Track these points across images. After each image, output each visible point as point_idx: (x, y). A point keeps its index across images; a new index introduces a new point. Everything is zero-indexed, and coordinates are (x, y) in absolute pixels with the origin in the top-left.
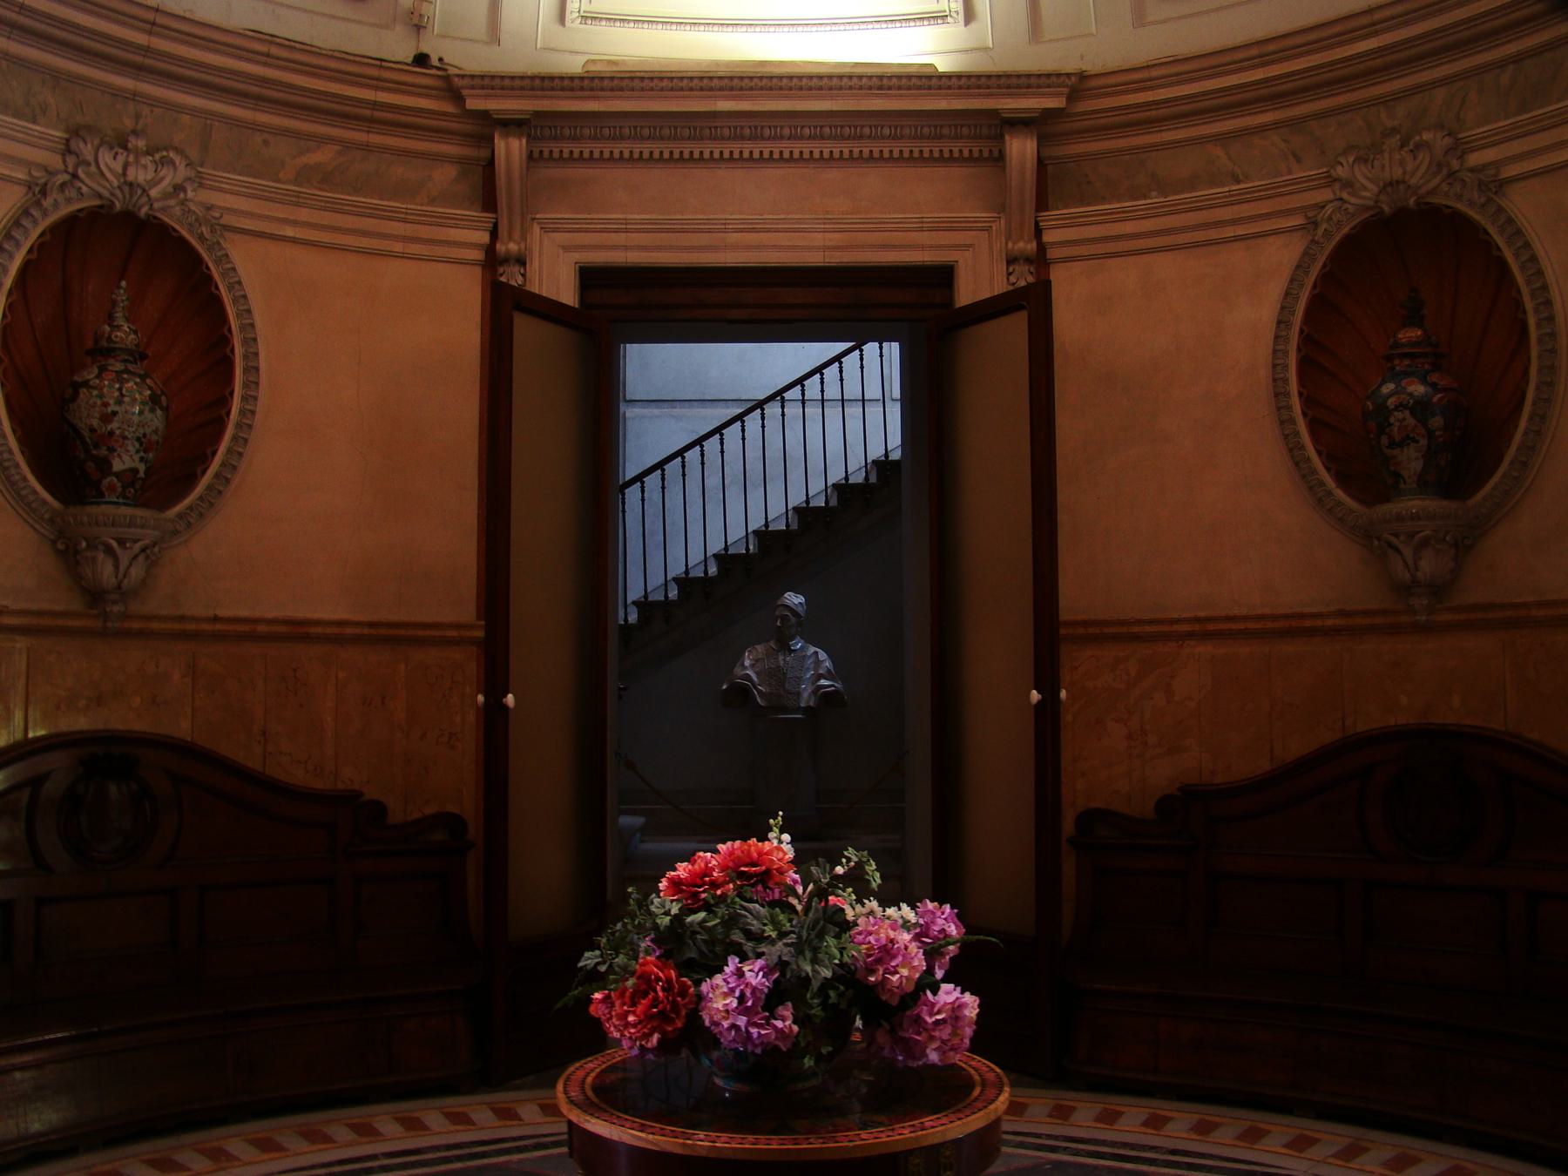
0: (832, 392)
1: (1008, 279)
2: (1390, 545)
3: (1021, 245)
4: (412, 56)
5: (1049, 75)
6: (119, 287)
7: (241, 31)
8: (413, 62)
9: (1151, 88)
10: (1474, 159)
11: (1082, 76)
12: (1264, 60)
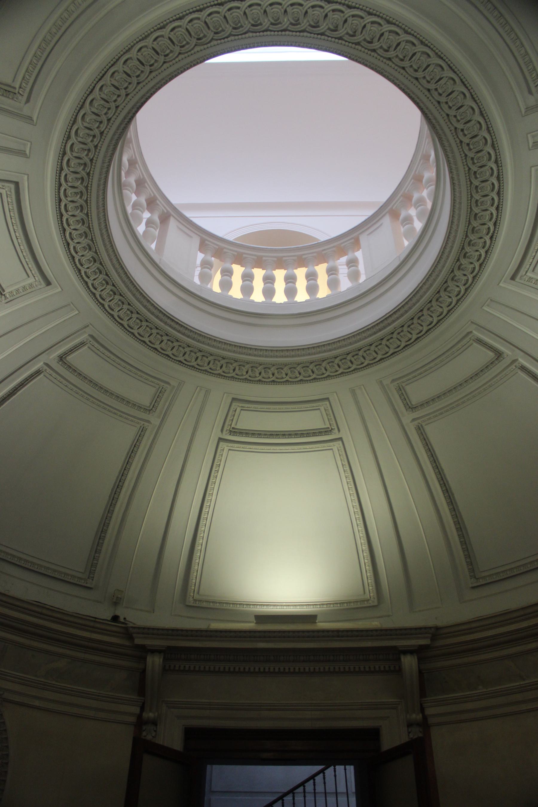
0: (320, 788)
1: (409, 735)
3: (414, 716)
4: (111, 616)
5: (420, 628)
7: (31, 602)
8: (111, 619)
9: (473, 633)
11: (437, 628)
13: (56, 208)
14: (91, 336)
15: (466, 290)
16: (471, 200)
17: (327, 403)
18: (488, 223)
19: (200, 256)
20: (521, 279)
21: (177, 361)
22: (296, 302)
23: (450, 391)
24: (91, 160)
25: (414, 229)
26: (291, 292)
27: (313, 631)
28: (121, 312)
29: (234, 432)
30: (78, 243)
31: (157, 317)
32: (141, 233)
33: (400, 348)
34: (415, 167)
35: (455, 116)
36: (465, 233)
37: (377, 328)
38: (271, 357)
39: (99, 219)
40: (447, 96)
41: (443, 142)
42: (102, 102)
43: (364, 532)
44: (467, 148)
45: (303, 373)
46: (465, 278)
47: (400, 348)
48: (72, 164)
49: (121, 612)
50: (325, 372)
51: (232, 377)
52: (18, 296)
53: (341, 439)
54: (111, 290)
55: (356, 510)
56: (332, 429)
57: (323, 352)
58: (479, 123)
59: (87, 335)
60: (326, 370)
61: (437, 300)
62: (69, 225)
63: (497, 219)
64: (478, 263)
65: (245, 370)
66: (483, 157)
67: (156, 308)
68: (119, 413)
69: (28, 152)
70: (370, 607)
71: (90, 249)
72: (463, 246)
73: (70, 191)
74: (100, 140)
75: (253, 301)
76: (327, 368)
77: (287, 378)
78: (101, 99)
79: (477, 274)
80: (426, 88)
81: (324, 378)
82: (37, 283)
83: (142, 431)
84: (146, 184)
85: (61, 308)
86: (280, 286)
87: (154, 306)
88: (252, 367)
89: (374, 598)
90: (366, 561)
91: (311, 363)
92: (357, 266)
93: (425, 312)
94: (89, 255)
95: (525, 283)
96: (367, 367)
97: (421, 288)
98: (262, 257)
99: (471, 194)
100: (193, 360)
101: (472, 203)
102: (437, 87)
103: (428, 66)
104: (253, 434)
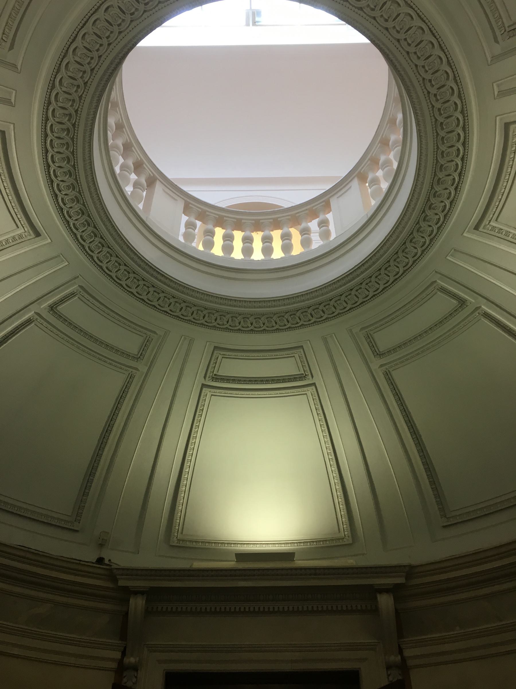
1: (388, 678)
7: (15, 546)
8: (96, 562)
11: (411, 567)
13: (43, 158)
14: (81, 287)
15: (431, 240)
16: (437, 151)
17: (302, 350)
18: (453, 174)
19: (185, 218)
20: (484, 228)
21: (163, 311)
22: (273, 259)
23: (415, 338)
24: (76, 111)
25: (381, 189)
26: (267, 250)
27: (291, 569)
28: (109, 264)
29: (216, 378)
30: (66, 195)
31: (144, 269)
32: (129, 193)
33: (368, 298)
34: (382, 132)
35: (423, 67)
36: (431, 184)
37: (347, 279)
38: (250, 307)
39: (85, 170)
40: (416, 46)
41: (411, 94)
42: (85, 51)
43: (337, 472)
44: (435, 99)
45: (278, 322)
46: (431, 229)
47: (368, 298)
48: (57, 114)
49: (107, 555)
50: (299, 321)
51: (214, 326)
52: (8, 245)
53: (314, 384)
54: (100, 243)
55: (329, 451)
56: (306, 375)
57: (297, 303)
58: (447, 73)
59: (77, 285)
60: (300, 319)
61: (403, 251)
62: (56, 177)
63: (462, 169)
64: (436, 226)
65: (225, 320)
66: (450, 107)
67: (143, 261)
68: (109, 361)
69: (13, 101)
70: (346, 545)
71: (78, 202)
72: (429, 198)
73: (56, 142)
74: (84, 91)
75: (233, 259)
76: (301, 318)
77: (265, 327)
78: (83, 48)
79: (442, 225)
80: (395, 39)
81: (298, 327)
82: (26, 234)
83: (131, 377)
84: (133, 148)
85: (51, 259)
86: (257, 245)
87: (141, 259)
88: (232, 317)
89: (349, 537)
90: (340, 500)
91: (286, 313)
92: (328, 226)
93: (392, 263)
94: (77, 207)
95: (488, 232)
96: (338, 316)
97: (388, 240)
98: (242, 219)
99: (437, 146)
100: (178, 310)
101: (438, 154)
102: (406, 37)
103: (398, 15)
104: (234, 380)
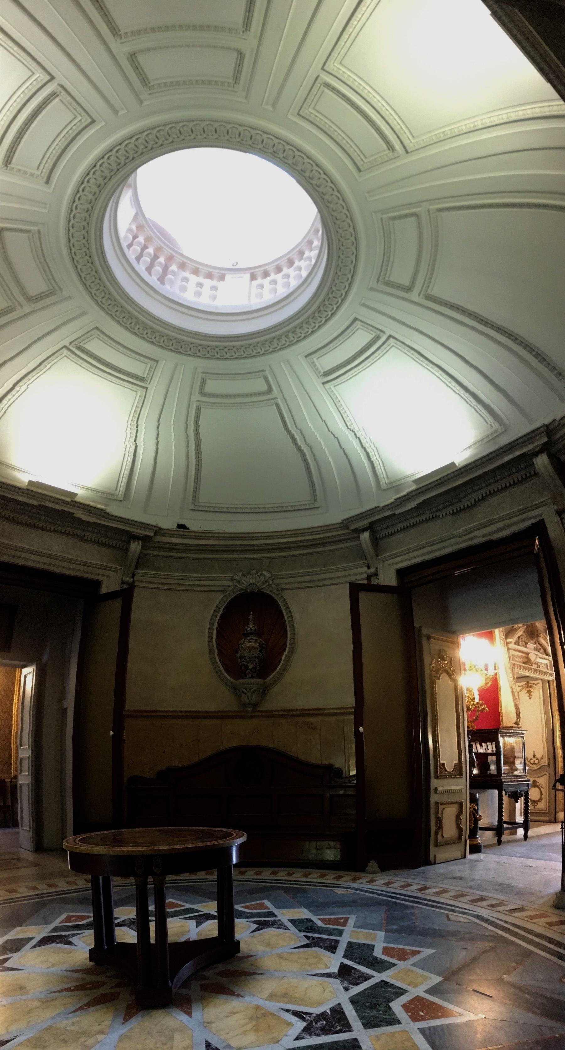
2: (243, 692)
3: (127, 579)
6: (250, 614)
10: (277, 581)
12: (289, 536)
14: (39, 232)
53: (390, 336)
